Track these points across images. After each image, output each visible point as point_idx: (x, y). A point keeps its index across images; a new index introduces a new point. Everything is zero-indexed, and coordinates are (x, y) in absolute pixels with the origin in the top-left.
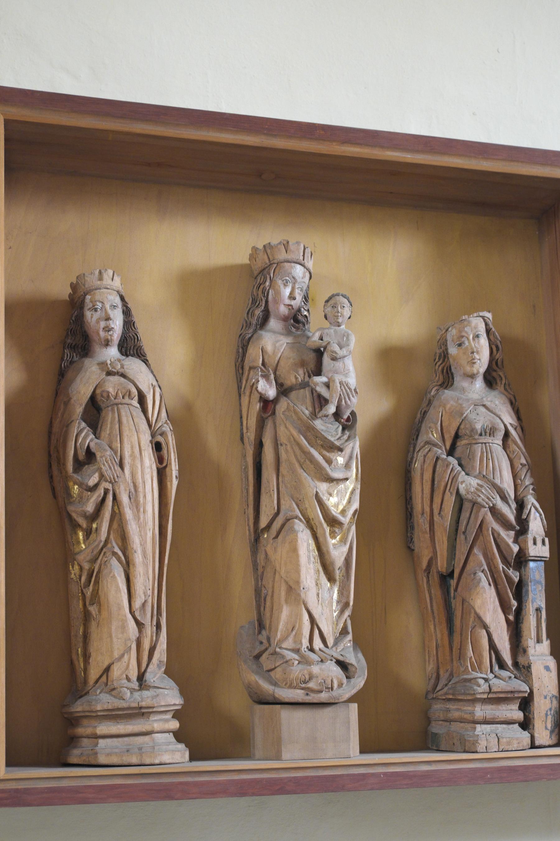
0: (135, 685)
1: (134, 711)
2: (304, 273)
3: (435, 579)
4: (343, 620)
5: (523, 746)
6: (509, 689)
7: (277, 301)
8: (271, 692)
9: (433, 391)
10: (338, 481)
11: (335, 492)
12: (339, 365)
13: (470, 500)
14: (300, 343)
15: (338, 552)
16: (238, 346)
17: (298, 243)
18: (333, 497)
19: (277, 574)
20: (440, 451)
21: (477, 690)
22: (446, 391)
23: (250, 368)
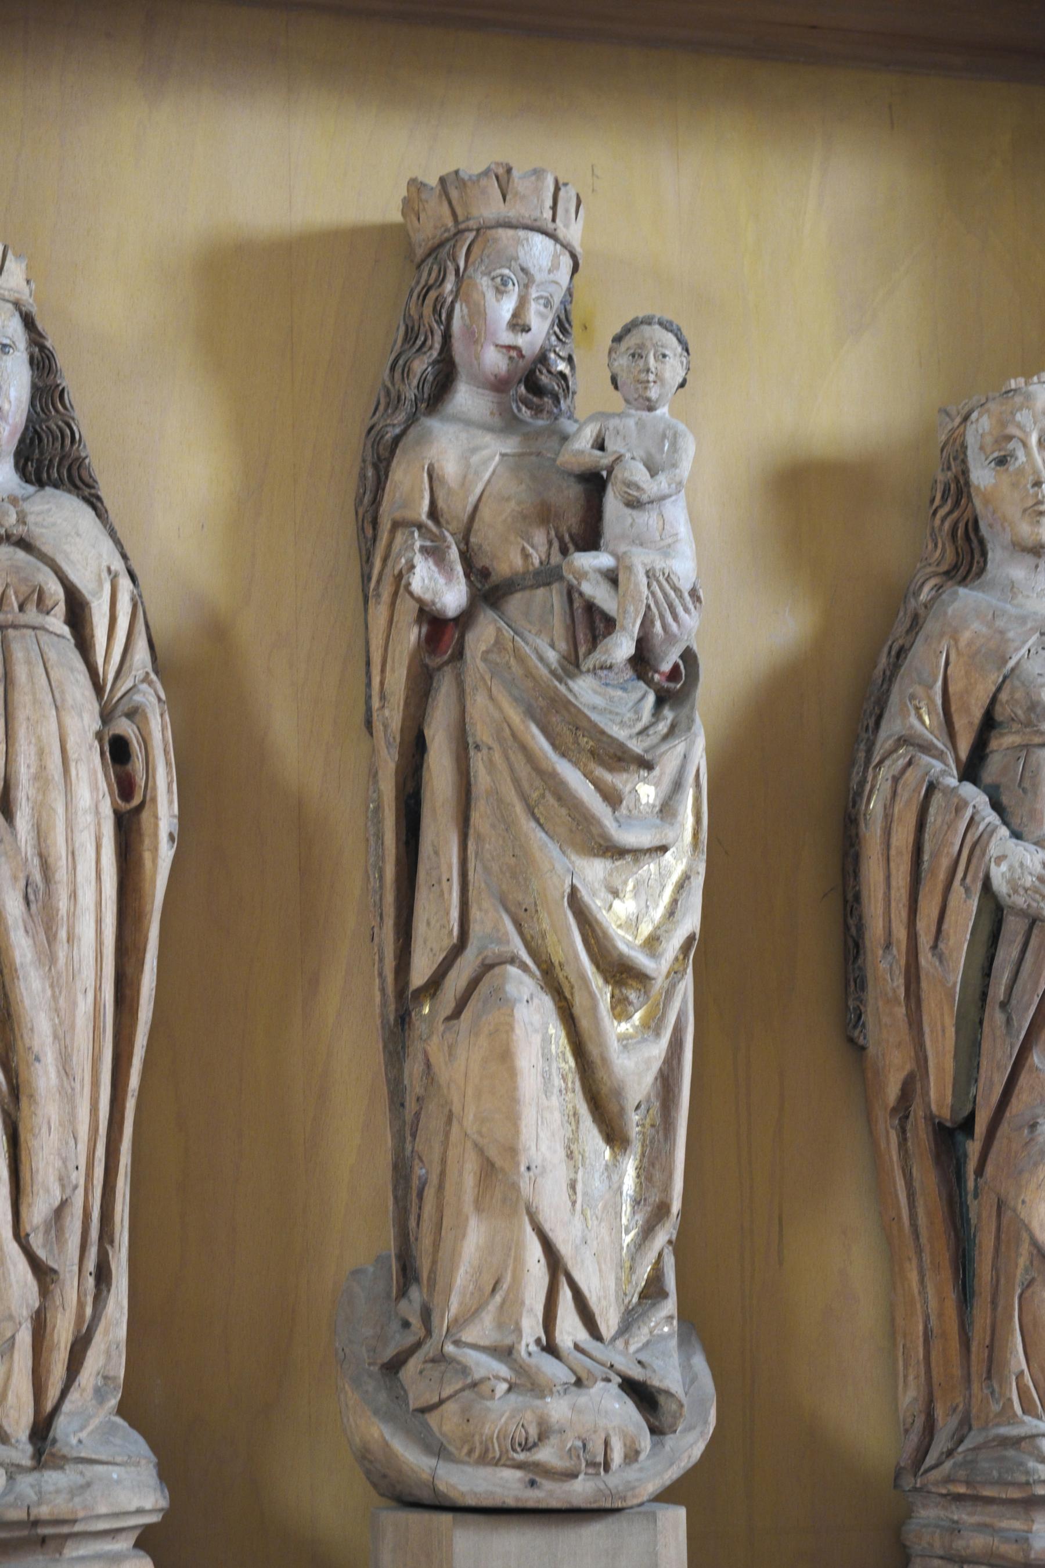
0: (22, 1452)
1: (17, 1534)
2: (556, 257)
3: (921, 1136)
4: (651, 1256)
7: (474, 338)
8: (425, 1476)
9: (926, 589)
10: (638, 854)
11: (631, 884)
12: (648, 519)
13: (1021, 910)
14: (539, 454)
15: (634, 1057)
16: (364, 461)
17: (538, 173)
18: (622, 900)
19: (455, 1123)
20: (938, 766)
21: (1035, 1471)
22: (962, 591)
23: (396, 525)
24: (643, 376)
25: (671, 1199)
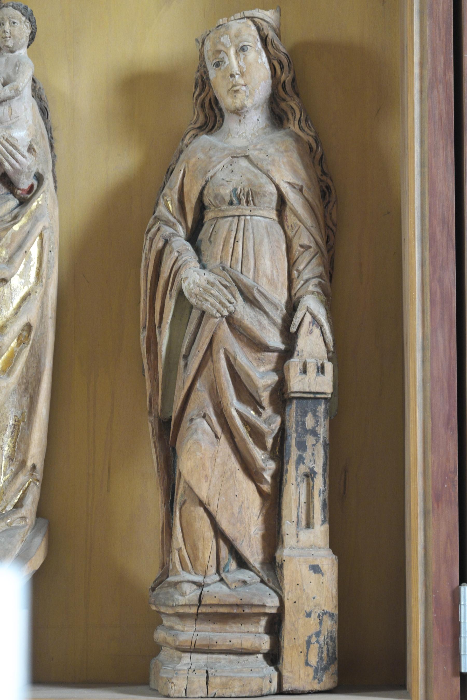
5: (251, 691)
6: (232, 600)
9: (188, 137)
21: (177, 600)
24: (3, 35)
25: (27, 459)
